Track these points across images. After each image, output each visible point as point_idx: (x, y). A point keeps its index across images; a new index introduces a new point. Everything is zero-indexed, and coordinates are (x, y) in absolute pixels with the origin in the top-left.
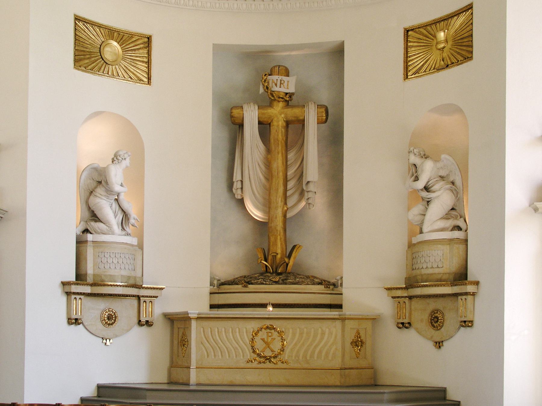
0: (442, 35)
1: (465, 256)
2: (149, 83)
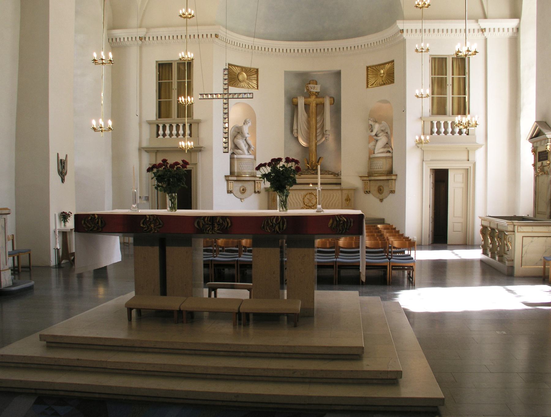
0: (382, 72)
1: (391, 164)
2: (257, 89)
